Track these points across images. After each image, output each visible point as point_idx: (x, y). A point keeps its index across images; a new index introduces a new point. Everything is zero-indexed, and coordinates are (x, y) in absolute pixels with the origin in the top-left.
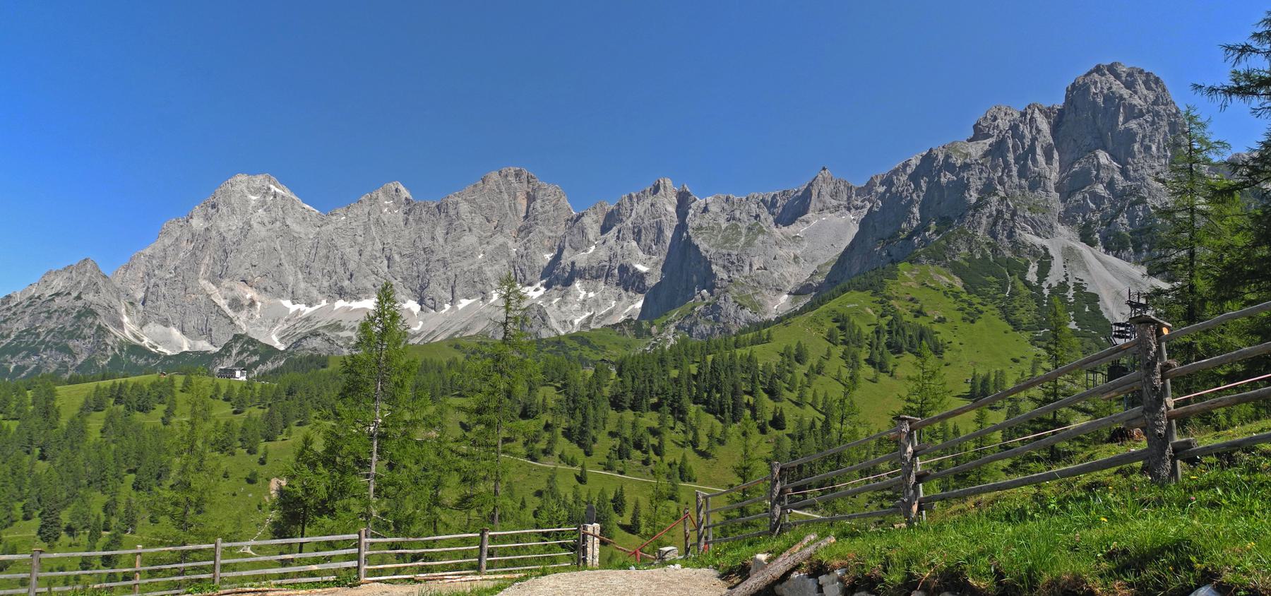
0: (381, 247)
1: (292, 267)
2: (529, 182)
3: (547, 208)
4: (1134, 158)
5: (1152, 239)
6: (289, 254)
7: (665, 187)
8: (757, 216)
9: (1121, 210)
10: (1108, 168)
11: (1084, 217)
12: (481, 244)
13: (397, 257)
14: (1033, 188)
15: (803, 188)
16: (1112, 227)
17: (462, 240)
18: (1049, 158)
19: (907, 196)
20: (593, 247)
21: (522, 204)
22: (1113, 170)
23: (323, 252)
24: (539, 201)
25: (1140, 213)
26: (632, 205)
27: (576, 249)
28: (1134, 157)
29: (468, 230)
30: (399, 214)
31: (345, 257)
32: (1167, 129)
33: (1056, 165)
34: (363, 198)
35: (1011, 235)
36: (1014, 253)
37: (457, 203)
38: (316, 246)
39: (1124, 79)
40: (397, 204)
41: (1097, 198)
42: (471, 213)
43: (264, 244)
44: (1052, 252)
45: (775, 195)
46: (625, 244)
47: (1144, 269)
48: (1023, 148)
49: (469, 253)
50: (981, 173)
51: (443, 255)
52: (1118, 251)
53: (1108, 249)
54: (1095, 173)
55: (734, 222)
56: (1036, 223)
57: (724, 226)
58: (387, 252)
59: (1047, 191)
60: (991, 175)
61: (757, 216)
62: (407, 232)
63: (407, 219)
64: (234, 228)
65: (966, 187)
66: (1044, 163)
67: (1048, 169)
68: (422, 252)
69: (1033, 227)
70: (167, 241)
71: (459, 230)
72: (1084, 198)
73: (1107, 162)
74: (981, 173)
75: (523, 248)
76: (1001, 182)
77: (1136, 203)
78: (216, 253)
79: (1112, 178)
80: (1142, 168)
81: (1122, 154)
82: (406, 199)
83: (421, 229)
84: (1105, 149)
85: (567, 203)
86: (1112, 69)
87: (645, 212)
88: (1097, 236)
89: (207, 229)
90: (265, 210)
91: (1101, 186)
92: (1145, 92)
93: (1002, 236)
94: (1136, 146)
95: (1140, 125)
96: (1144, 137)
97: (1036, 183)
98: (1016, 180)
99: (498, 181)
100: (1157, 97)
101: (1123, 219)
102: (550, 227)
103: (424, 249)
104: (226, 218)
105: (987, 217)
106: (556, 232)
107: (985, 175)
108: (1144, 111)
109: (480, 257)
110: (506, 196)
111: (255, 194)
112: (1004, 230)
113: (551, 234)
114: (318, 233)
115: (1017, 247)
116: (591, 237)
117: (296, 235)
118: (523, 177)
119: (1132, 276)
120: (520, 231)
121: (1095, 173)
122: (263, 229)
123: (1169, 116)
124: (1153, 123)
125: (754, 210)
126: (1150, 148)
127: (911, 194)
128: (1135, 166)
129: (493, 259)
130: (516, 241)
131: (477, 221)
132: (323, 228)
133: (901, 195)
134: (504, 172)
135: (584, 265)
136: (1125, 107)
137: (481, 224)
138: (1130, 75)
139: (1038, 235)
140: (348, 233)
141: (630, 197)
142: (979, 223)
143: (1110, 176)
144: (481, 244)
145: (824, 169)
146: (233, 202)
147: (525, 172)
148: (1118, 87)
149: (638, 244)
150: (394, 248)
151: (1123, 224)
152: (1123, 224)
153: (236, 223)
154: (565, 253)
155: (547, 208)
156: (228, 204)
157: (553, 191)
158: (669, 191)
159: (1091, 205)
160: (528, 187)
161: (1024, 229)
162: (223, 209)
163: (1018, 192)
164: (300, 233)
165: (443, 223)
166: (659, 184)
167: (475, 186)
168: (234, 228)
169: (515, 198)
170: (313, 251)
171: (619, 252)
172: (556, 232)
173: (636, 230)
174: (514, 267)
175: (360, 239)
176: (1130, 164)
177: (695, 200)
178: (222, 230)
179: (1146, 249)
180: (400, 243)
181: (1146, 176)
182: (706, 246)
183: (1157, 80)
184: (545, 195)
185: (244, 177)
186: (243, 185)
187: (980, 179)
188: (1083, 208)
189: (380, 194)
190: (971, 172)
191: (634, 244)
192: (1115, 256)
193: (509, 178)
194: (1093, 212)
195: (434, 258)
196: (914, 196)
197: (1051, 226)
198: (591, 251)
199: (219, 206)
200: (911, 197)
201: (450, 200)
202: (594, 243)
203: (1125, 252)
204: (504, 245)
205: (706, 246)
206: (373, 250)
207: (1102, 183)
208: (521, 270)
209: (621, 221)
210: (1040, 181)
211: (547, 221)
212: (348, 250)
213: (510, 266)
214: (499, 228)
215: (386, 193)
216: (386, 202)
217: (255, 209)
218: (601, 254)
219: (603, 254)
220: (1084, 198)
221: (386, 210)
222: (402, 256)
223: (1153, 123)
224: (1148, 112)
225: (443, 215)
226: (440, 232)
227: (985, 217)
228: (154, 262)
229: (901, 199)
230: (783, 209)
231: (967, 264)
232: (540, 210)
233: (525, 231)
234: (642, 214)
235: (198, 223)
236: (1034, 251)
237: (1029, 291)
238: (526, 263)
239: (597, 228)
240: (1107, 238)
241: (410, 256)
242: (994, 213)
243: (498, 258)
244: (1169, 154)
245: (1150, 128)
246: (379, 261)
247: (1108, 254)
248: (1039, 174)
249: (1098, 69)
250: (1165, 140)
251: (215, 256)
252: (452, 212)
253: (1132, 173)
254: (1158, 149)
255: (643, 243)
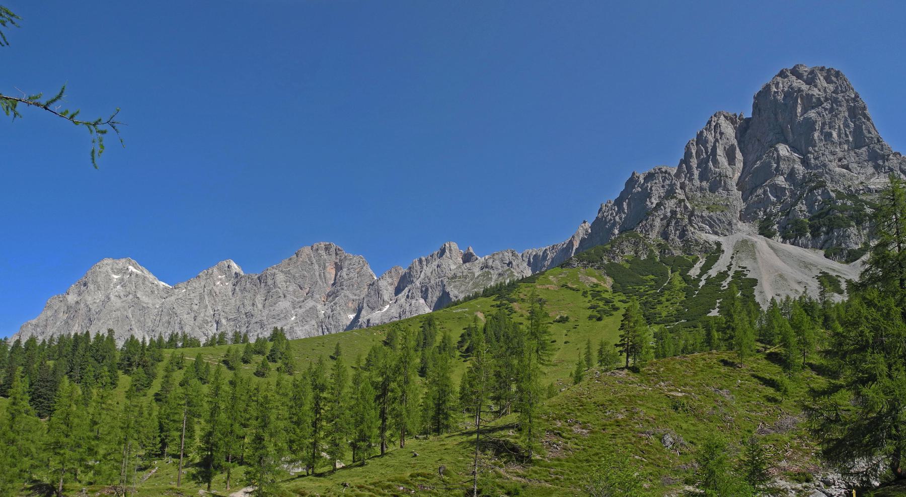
0: (212, 313)
1: (140, 331)
2: (337, 254)
3: (351, 275)
4: (815, 146)
5: (830, 220)
6: (139, 321)
7: (450, 250)
8: (510, 263)
9: (800, 198)
10: (788, 159)
11: (765, 212)
12: (294, 308)
13: (224, 321)
14: (713, 189)
15: (567, 242)
16: (791, 216)
17: (277, 305)
18: (731, 160)
19: (611, 220)
20: (388, 306)
21: (331, 272)
22: (794, 160)
23: (165, 318)
24: (345, 269)
25: (819, 198)
26: (422, 268)
27: (373, 309)
28: (814, 146)
29: (282, 296)
30: (229, 285)
31: (183, 322)
32: (846, 114)
33: (739, 165)
34: (201, 274)
35: (683, 234)
36: (685, 252)
37: (274, 274)
38: (160, 314)
39: (805, 77)
40: (228, 278)
41: (778, 191)
42: (286, 282)
43: (119, 313)
44: (723, 247)
45: (546, 250)
46: (413, 301)
47: (822, 252)
48: (707, 153)
49: (283, 315)
50: (664, 181)
51: (261, 318)
52: (796, 238)
53: (785, 238)
54: (775, 165)
55: (487, 270)
56: (714, 221)
57: (477, 275)
58: (217, 318)
59: (728, 190)
60: (674, 181)
61: (510, 263)
62: (233, 301)
63: (235, 289)
64: (98, 301)
65: (649, 196)
66: (726, 164)
67: (730, 169)
68: (244, 316)
69: (711, 226)
70: (49, 313)
71: (275, 297)
72: (765, 192)
73: (787, 154)
74: (664, 181)
75: (330, 310)
76: (683, 187)
77: (815, 188)
78: (83, 322)
79: (793, 168)
80: (823, 155)
81: (802, 147)
82: (236, 273)
83: (245, 297)
84: (785, 142)
85: (370, 270)
86: (795, 72)
87: (432, 273)
88: (775, 227)
89: (77, 303)
90: (122, 286)
91: (781, 178)
92: (825, 85)
93: (674, 235)
94: (816, 135)
95: (819, 113)
96: (824, 124)
97: (717, 183)
98: (697, 183)
99: (310, 254)
100: (837, 88)
101: (802, 206)
102: (354, 292)
103: (246, 313)
104: (93, 293)
105: (662, 220)
106: (359, 296)
107: (668, 182)
108: (822, 99)
109: (293, 319)
110: (316, 267)
111: (117, 274)
112: (676, 230)
113: (355, 298)
114: (163, 304)
115: (687, 245)
116: (386, 298)
117: (144, 305)
118: (332, 250)
119: (803, 260)
120: (328, 296)
121: (775, 165)
122: (119, 301)
123: (847, 101)
124: (831, 110)
125: (507, 258)
126: (831, 134)
127: (614, 217)
128: (816, 154)
129: (303, 320)
130: (325, 305)
131: (291, 289)
132: (167, 299)
133: (606, 218)
134: (315, 247)
135: (377, 322)
136: (802, 99)
137: (294, 291)
138: (812, 72)
139: (716, 233)
140: (187, 303)
141: (420, 261)
142: (652, 226)
143: (790, 167)
144: (294, 308)
145: (585, 222)
146: (99, 280)
147: (334, 246)
148: (797, 83)
149: (425, 301)
150: (222, 313)
151: (801, 211)
152: (801, 211)
153: (100, 296)
154: (363, 312)
155: (351, 275)
156: (95, 282)
157: (357, 260)
158: (454, 254)
159: (772, 198)
160: (336, 259)
161: (701, 229)
162: (91, 286)
163: (699, 194)
164: (148, 303)
165: (263, 291)
166: (445, 248)
167: (290, 259)
168: (98, 301)
169: (325, 268)
170: (158, 318)
171: (407, 308)
172: (359, 296)
173: (424, 289)
174: (322, 326)
175: (195, 307)
176: (811, 153)
177: (477, 259)
178: (88, 303)
179: (823, 232)
180: (227, 309)
181: (827, 162)
182: (456, 292)
183: (838, 74)
184: (350, 264)
185: (108, 261)
186: (108, 267)
187: (663, 186)
188: (764, 203)
189: (215, 270)
190: (654, 181)
191: (422, 301)
192: (793, 244)
193: (320, 251)
194: (774, 204)
195: (254, 320)
196: (617, 218)
197: (730, 224)
198: (385, 309)
199: (89, 284)
200: (614, 219)
201: (268, 272)
202: (388, 303)
203: (803, 238)
204: (314, 308)
205: (456, 292)
206: (205, 316)
207: (782, 174)
208: (328, 329)
209: (412, 282)
210: (721, 180)
211: (351, 287)
212: (185, 316)
213: (318, 326)
214: (310, 294)
215: (219, 269)
216: (220, 277)
217: (116, 284)
218: (392, 311)
219: (395, 312)
220: (765, 192)
221: (218, 283)
222: (228, 320)
223: (831, 110)
224: (826, 99)
225: (263, 285)
226: (259, 299)
227: (658, 220)
228: (38, 329)
229: (606, 223)
230: (552, 261)
231: (627, 266)
232: (346, 277)
233: (332, 295)
234: (429, 274)
235: (72, 298)
236: (706, 248)
237: (684, 285)
238: (332, 323)
239: (391, 289)
240: (785, 228)
241: (235, 320)
242: (669, 214)
243: (309, 320)
244: (851, 139)
245: (830, 116)
246: (210, 324)
247: (785, 243)
248: (720, 174)
249: (782, 74)
250: (846, 126)
251: (83, 324)
252: (270, 282)
253: (812, 161)
254: (839, 136)
255: (429, 300)
